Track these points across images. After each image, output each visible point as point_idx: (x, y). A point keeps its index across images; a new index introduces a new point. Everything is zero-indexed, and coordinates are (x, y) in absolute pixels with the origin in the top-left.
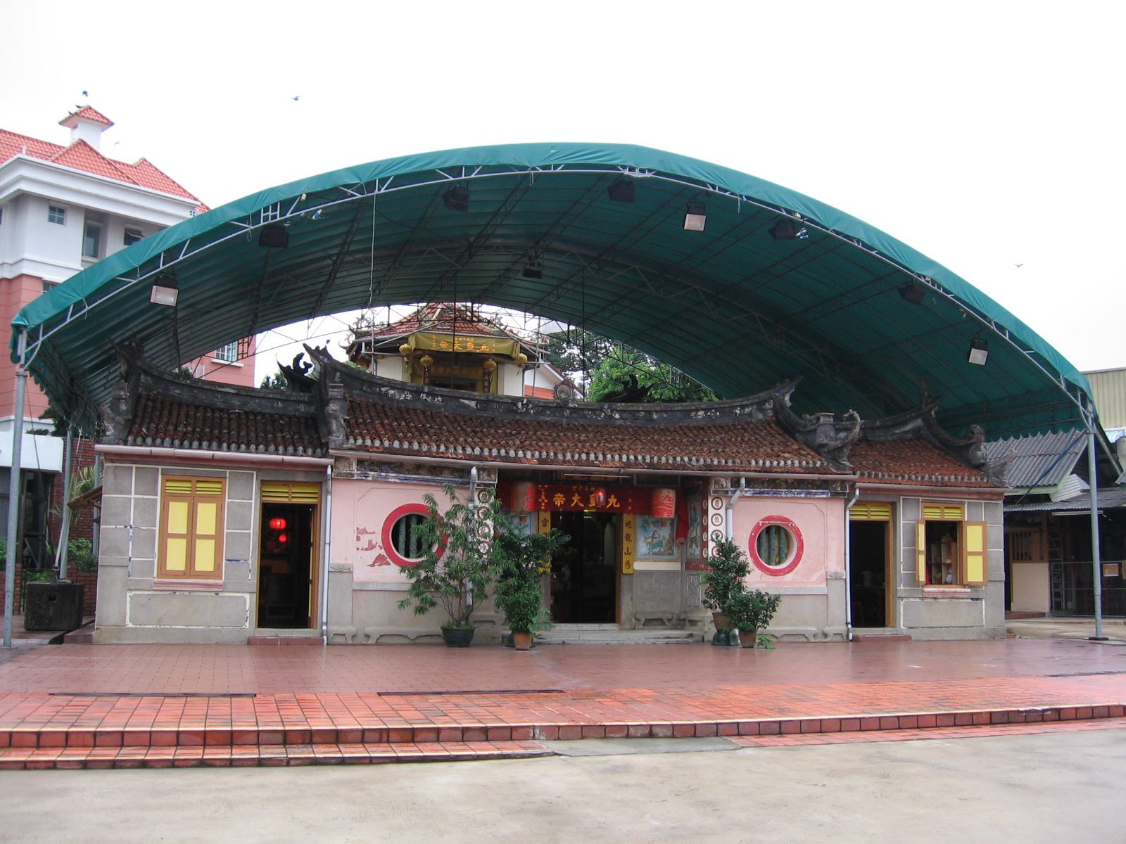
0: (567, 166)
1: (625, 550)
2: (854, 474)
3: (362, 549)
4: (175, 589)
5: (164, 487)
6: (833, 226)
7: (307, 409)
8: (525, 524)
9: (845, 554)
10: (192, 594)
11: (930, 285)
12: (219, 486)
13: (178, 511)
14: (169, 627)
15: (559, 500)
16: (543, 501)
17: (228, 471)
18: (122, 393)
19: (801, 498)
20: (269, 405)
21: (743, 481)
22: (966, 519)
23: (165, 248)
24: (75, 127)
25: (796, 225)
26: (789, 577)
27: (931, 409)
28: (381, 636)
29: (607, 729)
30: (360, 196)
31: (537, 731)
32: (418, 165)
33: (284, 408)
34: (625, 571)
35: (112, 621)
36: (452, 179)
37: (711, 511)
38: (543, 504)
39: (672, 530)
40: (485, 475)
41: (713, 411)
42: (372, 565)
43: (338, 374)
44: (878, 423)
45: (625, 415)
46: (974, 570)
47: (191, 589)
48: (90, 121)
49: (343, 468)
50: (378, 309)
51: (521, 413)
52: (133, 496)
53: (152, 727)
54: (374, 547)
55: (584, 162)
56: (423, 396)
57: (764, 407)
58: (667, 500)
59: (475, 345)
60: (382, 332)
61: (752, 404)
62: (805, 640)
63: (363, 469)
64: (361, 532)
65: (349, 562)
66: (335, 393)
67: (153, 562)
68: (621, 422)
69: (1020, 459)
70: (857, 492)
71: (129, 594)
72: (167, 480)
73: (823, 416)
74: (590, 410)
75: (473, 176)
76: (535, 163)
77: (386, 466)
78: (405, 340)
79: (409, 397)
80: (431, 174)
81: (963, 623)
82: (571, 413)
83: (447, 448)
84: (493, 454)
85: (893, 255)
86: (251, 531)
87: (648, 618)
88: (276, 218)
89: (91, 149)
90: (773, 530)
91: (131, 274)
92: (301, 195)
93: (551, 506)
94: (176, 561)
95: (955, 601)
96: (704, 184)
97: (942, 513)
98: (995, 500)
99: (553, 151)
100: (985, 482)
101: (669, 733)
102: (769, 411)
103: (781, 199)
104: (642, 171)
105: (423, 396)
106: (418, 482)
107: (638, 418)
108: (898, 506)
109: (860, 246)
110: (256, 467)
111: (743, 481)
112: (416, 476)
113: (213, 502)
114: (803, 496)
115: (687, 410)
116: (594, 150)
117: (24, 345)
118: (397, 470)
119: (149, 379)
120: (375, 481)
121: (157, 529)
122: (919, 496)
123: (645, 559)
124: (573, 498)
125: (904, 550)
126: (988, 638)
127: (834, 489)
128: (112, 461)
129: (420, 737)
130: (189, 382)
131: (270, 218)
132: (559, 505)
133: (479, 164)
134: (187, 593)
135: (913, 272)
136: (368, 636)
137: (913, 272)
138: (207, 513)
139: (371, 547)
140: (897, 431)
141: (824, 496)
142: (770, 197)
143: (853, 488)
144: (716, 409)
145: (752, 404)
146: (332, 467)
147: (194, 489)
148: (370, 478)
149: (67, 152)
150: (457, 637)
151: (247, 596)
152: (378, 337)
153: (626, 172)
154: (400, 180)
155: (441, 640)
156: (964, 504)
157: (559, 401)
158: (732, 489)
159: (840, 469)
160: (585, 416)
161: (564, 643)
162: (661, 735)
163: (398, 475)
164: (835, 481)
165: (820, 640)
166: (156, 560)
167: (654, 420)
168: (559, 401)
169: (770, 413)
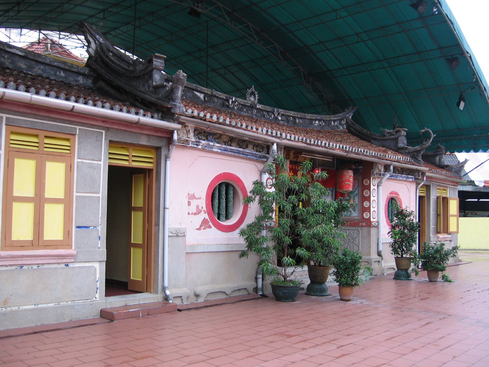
3: (192, 214)
4: (24, 262)
5: (8, 139)
7: (85, 81)
10: (41, 267)
13: (25, 169)
14: (16, 308)
17: (78, 127)
20: (53, 73)
21: (392, 168)
33: (66, 78)
42: (199, 229)
64: (192, 197)
65: (183, 226)
72: (13, 133)
77: (211, 137)
86: (100, 195)
111: (392, 168)
115: (311, 119)
120: (203, 150)
138: (55, 172)
144: (324, 120)
150: (283, 293)
151: (97, 265)
163: (221, 145)
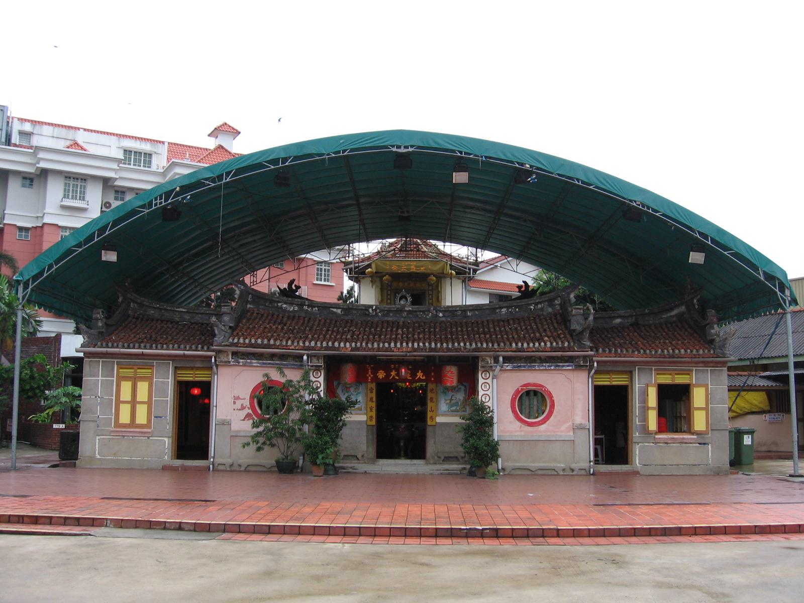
0: (352, 150)
1: (429, 409)
2: (591, 351)
6: (556, 171)
8: (359, 391)
9: (588, 410)
11: (640, 207)
12: (150, 371)
13: (126, 387)
15: (381, 375)
16: (370, 376)
17: (155, 362)
18: (98, 316)
19: (551, 370)
22: (694, 383)
23: (97, 228)
24: (217, 137)
25: (529, 173)
26: (543, 427)
27: (693, 299)
28: (248, 466)
29: (152, 523)
30: (213, 185)
31: (109, 522)
32: (251, 161)
34: (429, 422)
35: (88, 454)
36: (273, 167)
37: (481, 381)
38: (370, 378)
39: (465, 394)
40: (314, 360)
41: (513, 308)
42: (244, 420)
43: (250, 296)
44: (647, 311)
45: (447, 314)
46: (699, 421)
47: (133, 435)
48: (228, 133)
49: (223, 358)
50: (356, 244)
51: (372, 316)
52: (100, 378)
53: (376, 524)
54: (245, 408)
55: (364, 146)
56: (305, 308)
57: (554, 303)
58: (451, 374)
59: (416, 267)
61: (545, 301)
62: (556, 473)
63: (236, 358)
66: (226, 310)
67: (111, 418)
68: (444, 319)
69: (740, 336)
70: (595, 364)
71: (98, 438)
73: (575, 308)
74: (421, 311)
75: (287, 164)
76: (328, 151)
77: (251, 356)
79: (296, 308)
80: (260, 166)
81: (691, 462)
82: (407, 314)
84: (324, 346)
85: (608, 188)
86: (169, 399)
87: (447, 456)
88: (162, 203)
89: (226, 150)
90: (532, 393)
91: (79, 245)
92: (176, 188)
93: (375, 379)
94: (125, 418)
95: (684, 445)
96: (454, 151)
97: (673, 379)
98: (720, 367)
99: (341, 141)
100: (711, 353)
101: (192, 528)
102: (557, 306)
103: (513, 155)
104: (406, 147)
105: (305, 308)
106: (272, 366)
107: (457, 316)
108: (634, 373)
109: (580, 184)
110: (172, 358)
111: (501, 359)
112: (270, 362)
113: (130, 381)
114: (552, 368)
116: (372, 137)
117: (22, 291)
118: (259, 358)
119: (136, 305)
120: (244, 365)
121: (114, 398)
122: (692, 367)
123: (444, 414)
124: (418, 374)
125: (638, 406)
126: (713, 474)
127: (577, 362)
128: (89, 358)
129: (41, 521)
130: (158, 305)
131: (158, 203)
132: (381, 378)
133: (291, 155)
134: (131, 438)
135: (625, 199)
136: (240, 466)
137: (625, 199)
139: (243, 408)
140: (663, 316)
141: (571, 368)
142: (505, 155)
143: (592, 362)
144: (515, 306)
145: (545, 301)
146: (215, 358)
147: (135, 373)
148: (241, 364)
149: (212, 152)
150: (286, 468)
151: (166, 439)
153: (394, 149)
154: (239, 171)
155: (276, 469)
156: (692, 371)
157: (400, 306)
158: (495, 365)
159: (581, 347)
160: (417, 316)
161: (366, 472)
162: (186, 529)
164: (578, 357)
165: (568, 473)
166: (113, 417)
167: (469, 316)
168: (400, 306)
169: (558, 307)
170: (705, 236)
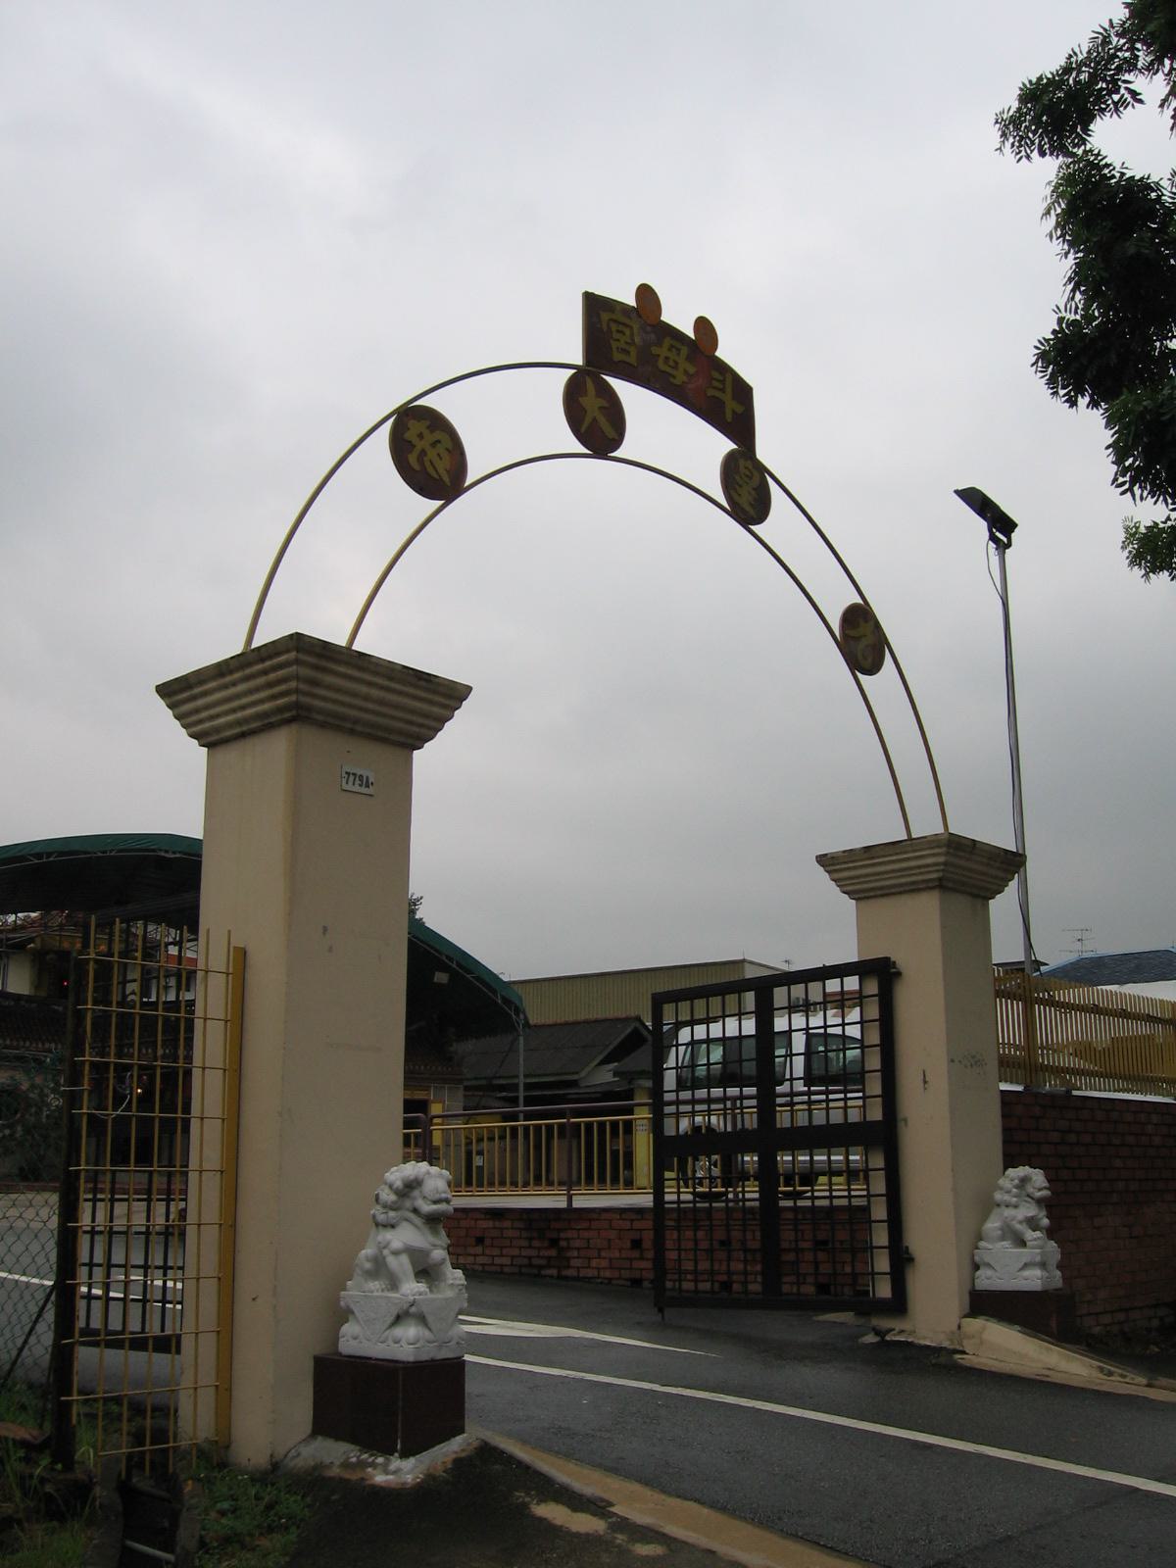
52: (157, 1114)
60: (10, 931)
78: (32, 940)
79: (12, 1003)
80: (22, 858)
83: (31, 1044)
152: (11, 936)
153: (163, 854)
170: (451, 959)
